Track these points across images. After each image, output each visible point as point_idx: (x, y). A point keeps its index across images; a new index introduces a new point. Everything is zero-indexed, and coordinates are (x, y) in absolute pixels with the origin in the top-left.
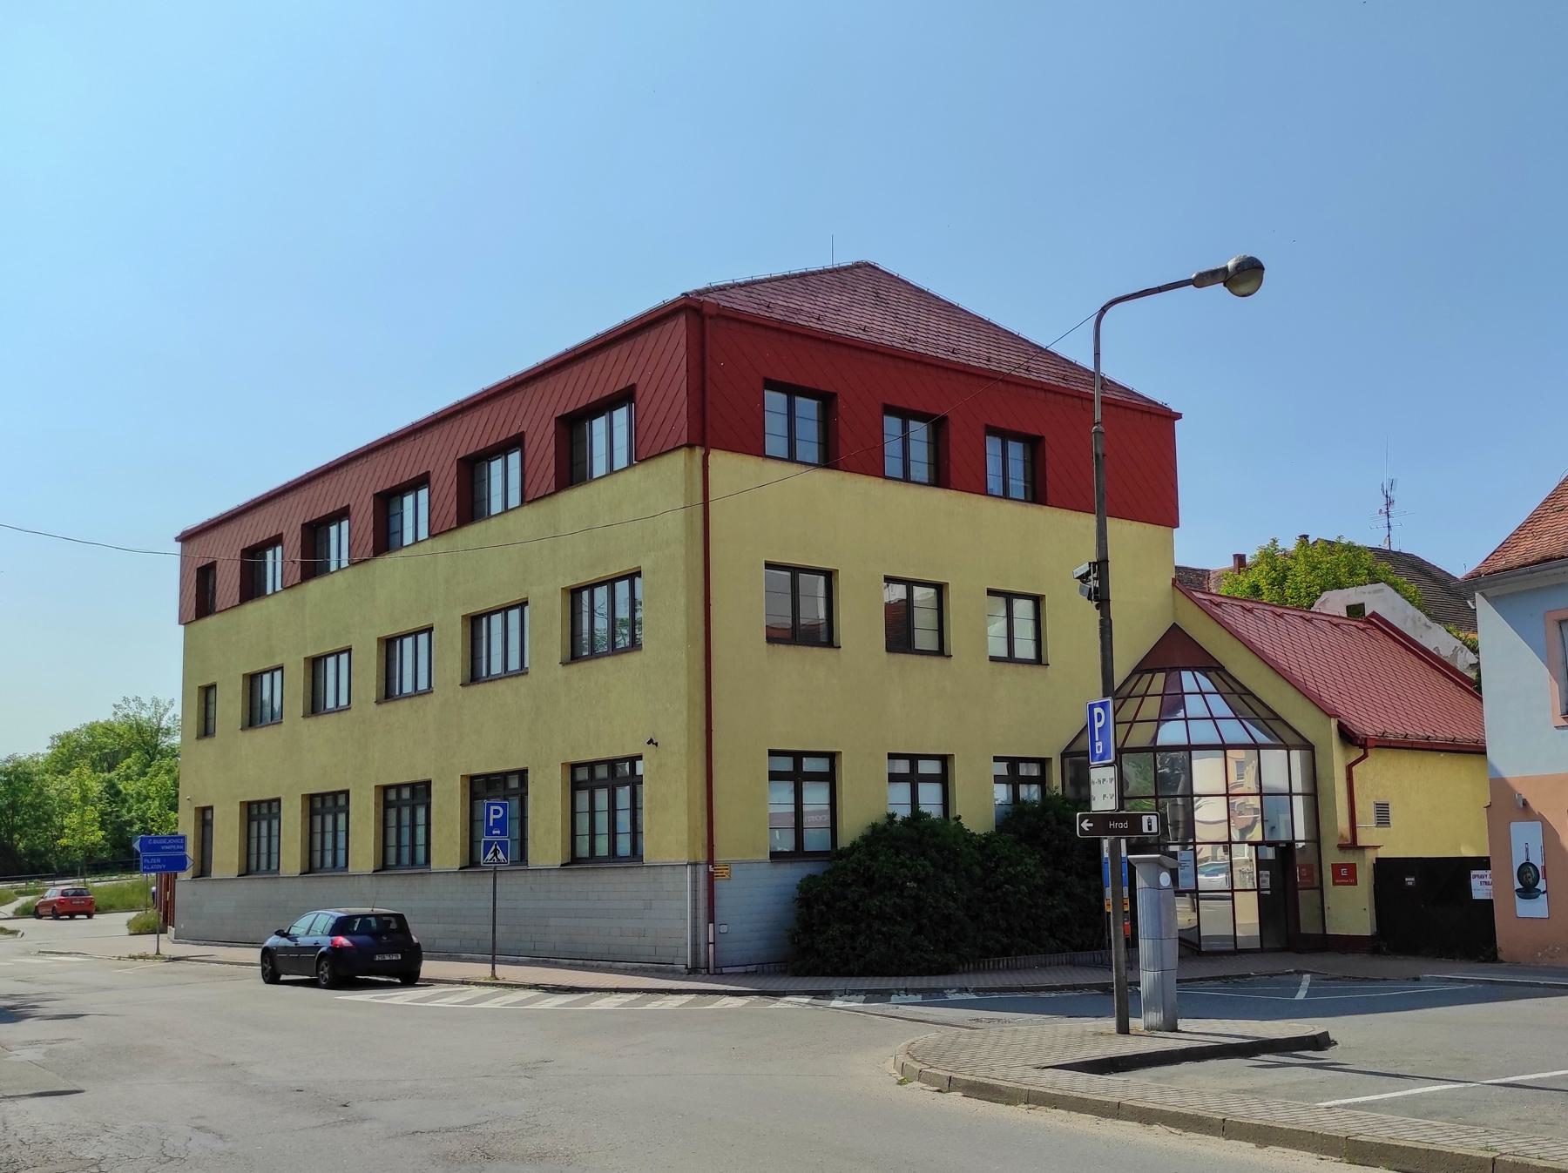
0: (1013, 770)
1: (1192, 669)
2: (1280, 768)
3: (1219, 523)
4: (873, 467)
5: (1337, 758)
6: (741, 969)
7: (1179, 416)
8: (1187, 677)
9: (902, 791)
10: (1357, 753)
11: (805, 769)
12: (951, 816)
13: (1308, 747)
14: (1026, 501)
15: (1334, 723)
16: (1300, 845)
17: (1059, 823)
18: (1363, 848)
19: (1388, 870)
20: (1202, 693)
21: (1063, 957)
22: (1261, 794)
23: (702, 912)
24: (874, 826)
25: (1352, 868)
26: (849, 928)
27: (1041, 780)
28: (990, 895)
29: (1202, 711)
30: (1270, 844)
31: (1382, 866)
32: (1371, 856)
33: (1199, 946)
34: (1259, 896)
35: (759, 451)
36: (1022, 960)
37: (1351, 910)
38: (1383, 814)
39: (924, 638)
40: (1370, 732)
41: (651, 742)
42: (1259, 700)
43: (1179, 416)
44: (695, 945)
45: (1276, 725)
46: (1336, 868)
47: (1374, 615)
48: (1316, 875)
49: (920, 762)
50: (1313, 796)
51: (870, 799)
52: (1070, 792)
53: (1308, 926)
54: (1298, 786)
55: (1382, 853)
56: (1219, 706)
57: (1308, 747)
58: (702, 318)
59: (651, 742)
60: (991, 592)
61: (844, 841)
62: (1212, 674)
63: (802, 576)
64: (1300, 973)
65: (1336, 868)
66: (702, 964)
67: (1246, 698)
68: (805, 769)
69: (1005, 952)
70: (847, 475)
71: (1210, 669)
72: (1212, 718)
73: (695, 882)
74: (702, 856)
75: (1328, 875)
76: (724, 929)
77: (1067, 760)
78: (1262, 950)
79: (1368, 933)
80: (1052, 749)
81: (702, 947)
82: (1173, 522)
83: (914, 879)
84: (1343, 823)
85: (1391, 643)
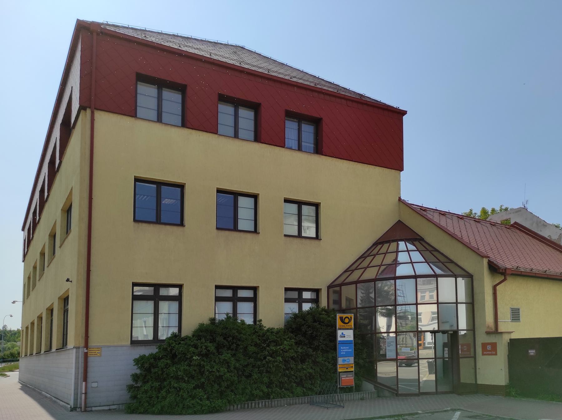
0: (294, 294)
1: (406, 240)
2: (450, 289)
3: (431, 177)
5: (487, 282)
7: (404, 113)
8: (402, 245)
9: (226, 308)
10: (500, 278)
11: (161, 294)
13: (469, 276)
14: (314, 153)
15: (485, 261)
16: (463, 333)
18: (501, 333)
19: (516, 345)
20: (408, 251)
21: (306, 399)
22: (438, 303)
23: (81, 376)
24: (201, 325)
25: (494, 346)
26: (157, 384)
27: (316, 301)
29: (408, 260)
30: (444, 332)
31: (514, 344)
32: (506, 338)
33: (397, 391)
34: (444, 360)
37: (494, 370)
38: (515, 315)
39: (245, 223)
40: (508, 266)
42: (442, 254)
43: (404, 113)
44: (76, 394)
45: (450, 266)
46: (484, 345)
47: (516, 223)
48: (472, 350)
49: (239, 291)
50: (471, 305)
51: (201, 309)
53: (465, 377)
54: (462, 297)
55: (514, 336)
56: (417, 256)
57: (469, 276)
60: (287, 201)
62: (417, 243)
63: (163, 187)
64: (454, 410)
65: (484, 345)
66: (79, 406)
67: (435, 253)
68: (161, 294)
69: (267, 396)
70: (194, 132)
71: (416, 240)
72: (412, 263)
74: (82, 344)
75: (479, 350)
76: (95, 385)
78: (437, 393)
79: (503, 383)
81: (79, 395)
84: (489, 319)
85: (524, 235)
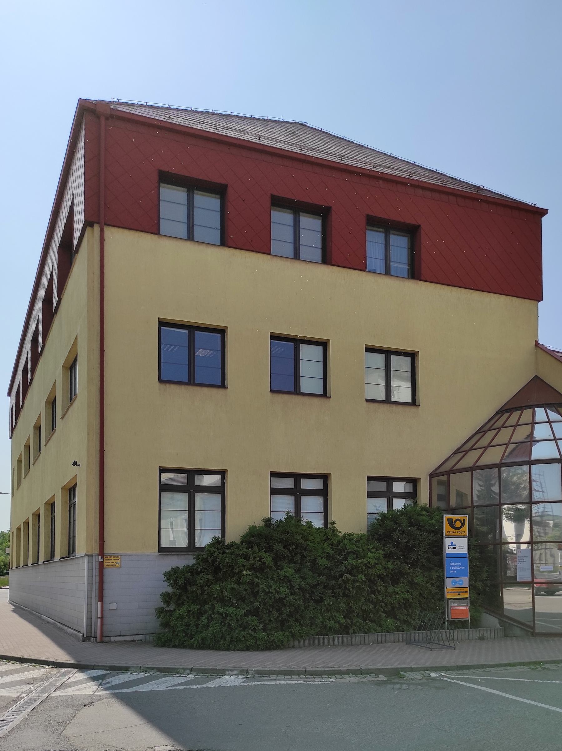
1: (546, 406)
4: (261, 245)
6: (129, 638)
7: (543, 212)
9: (285, 504)
12: (329, 521)
14: (408, 278)
17: (411, 525)
21: (400, 636)
23: (95, 593)
24: (253, 528)
26: (195, 608)
27: (412, 495)
28: (333, 582)
33: (533, 628)
35: (154, 229)
36: (357, 638)
39: (310, 382)
41: (75, 464)
44: (89, 619)
51: (251, 507)
52: (436, 504)
58: (98, 117)
59: (75, 464)
60: (369, 349)
61: (228, 541)
63: (197, 333)
66: (93, 635)
69: (345, 630)
70: (237, 252)
73: (90, 569)
74: (96, 551)
76: (113, 607)
77: (435, 480)
80: (422, 472)
82: (536, 295)
83: (251, 569)
